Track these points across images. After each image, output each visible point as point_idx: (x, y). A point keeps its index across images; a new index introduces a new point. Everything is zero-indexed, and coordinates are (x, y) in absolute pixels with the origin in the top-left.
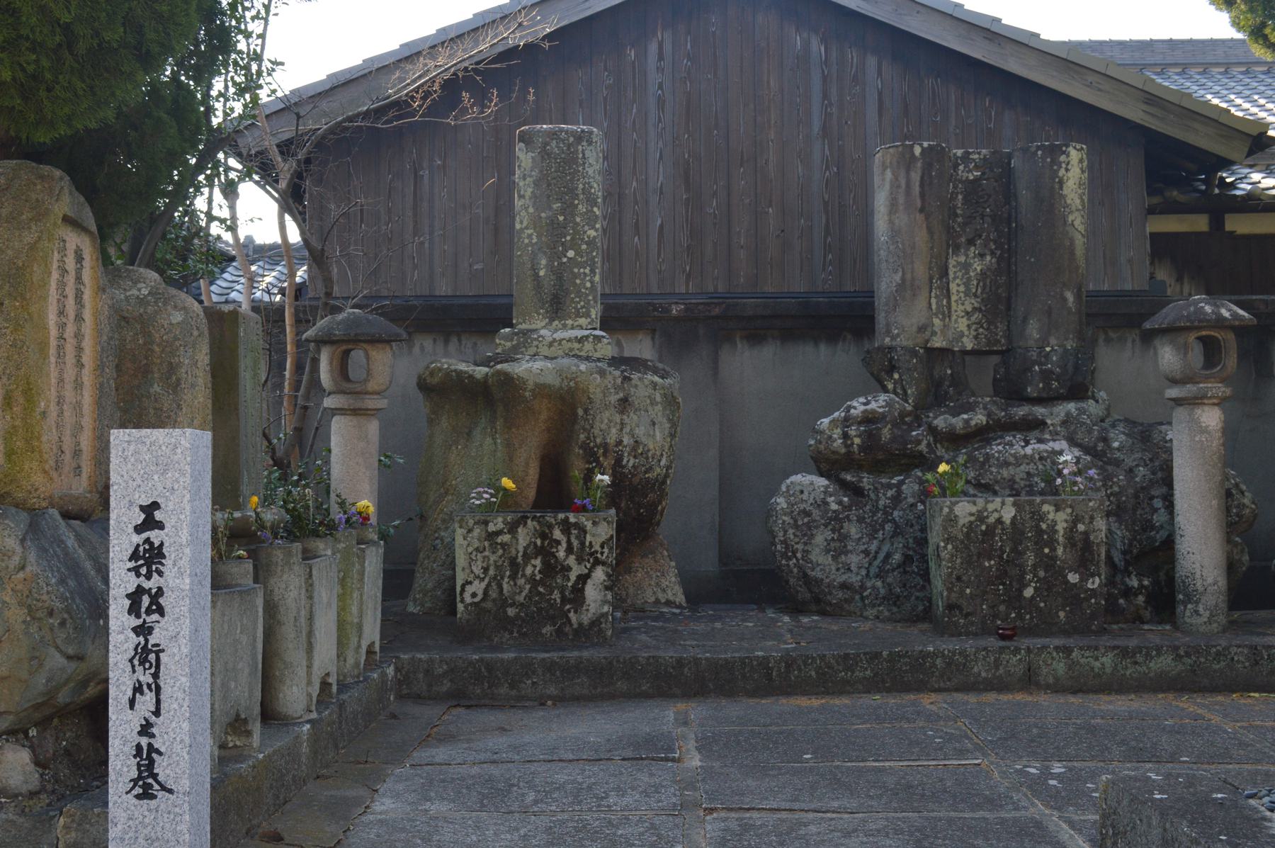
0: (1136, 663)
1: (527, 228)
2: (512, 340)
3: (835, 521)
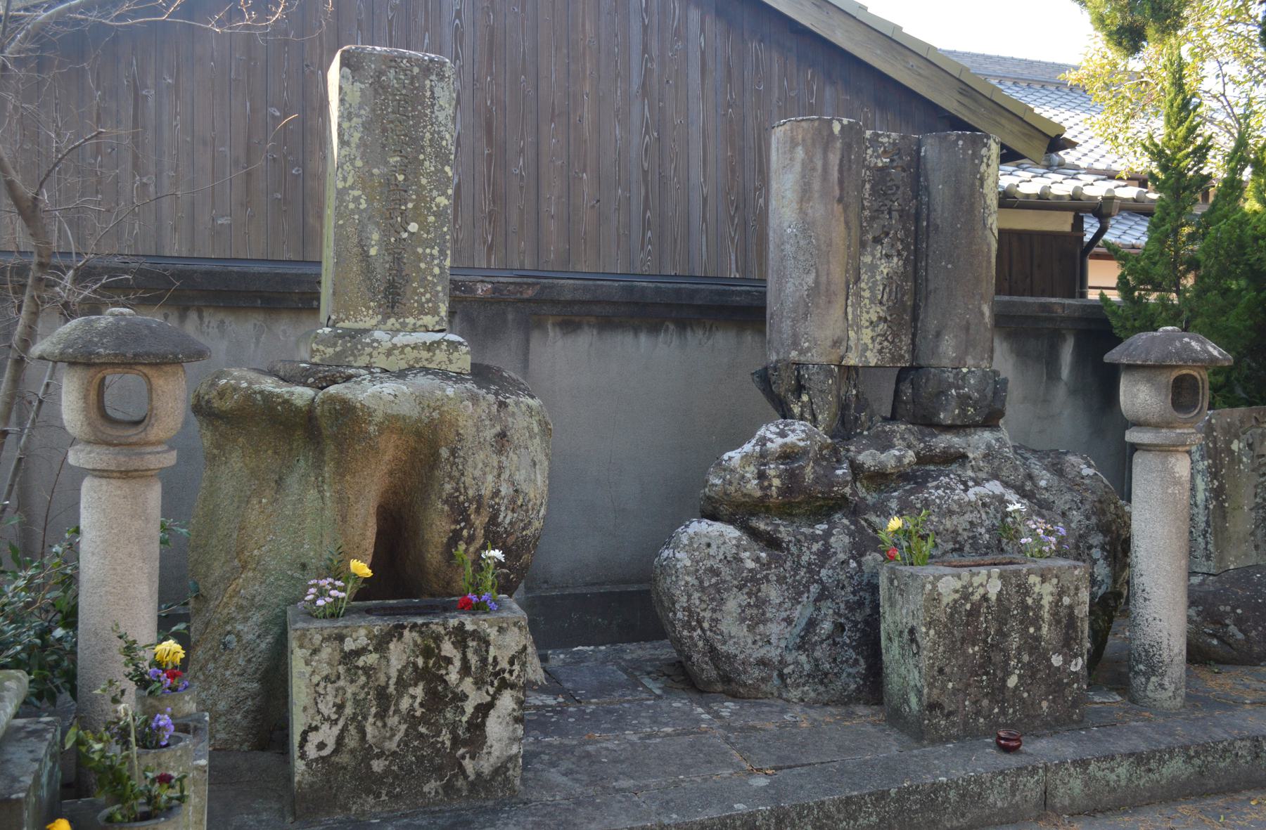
0: (1150, 770)
1: (352, 188)
2: (335, 345)
3: (751, 582)
